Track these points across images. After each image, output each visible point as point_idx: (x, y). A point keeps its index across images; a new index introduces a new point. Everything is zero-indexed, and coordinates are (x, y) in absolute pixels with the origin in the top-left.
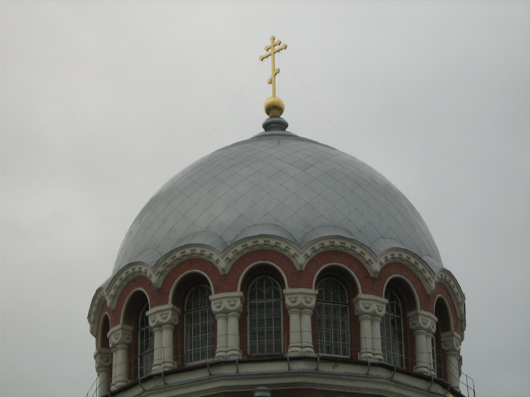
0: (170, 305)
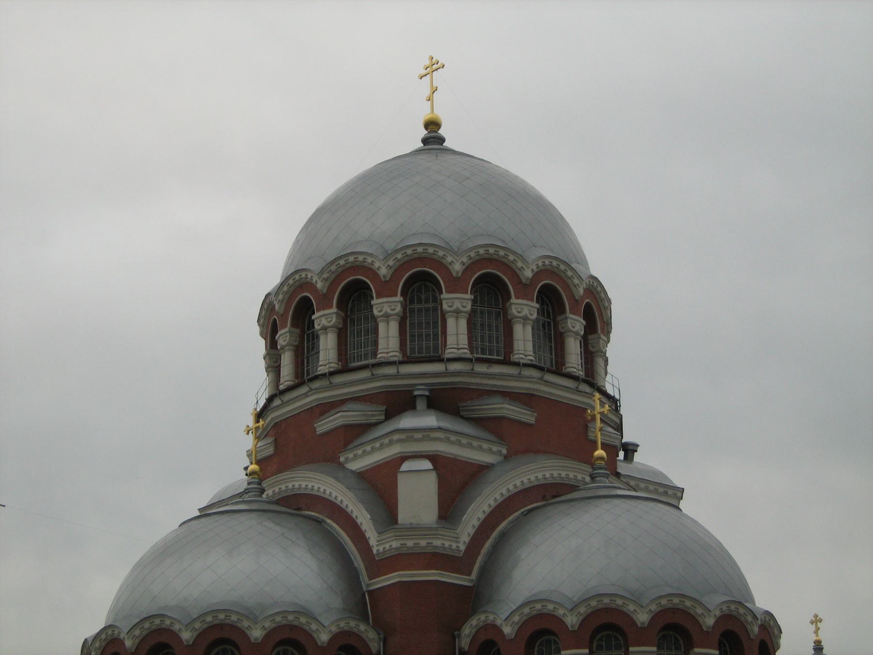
0: (334, 310)
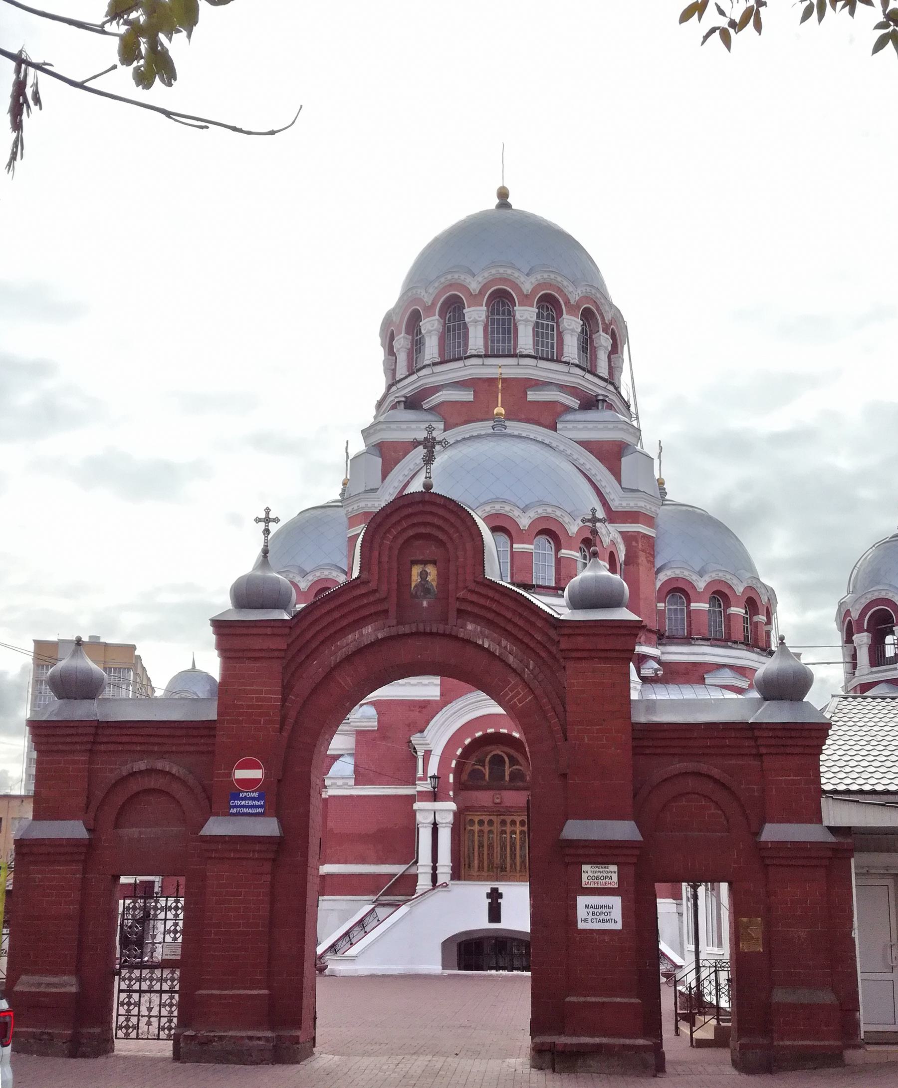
0: (437, 317)
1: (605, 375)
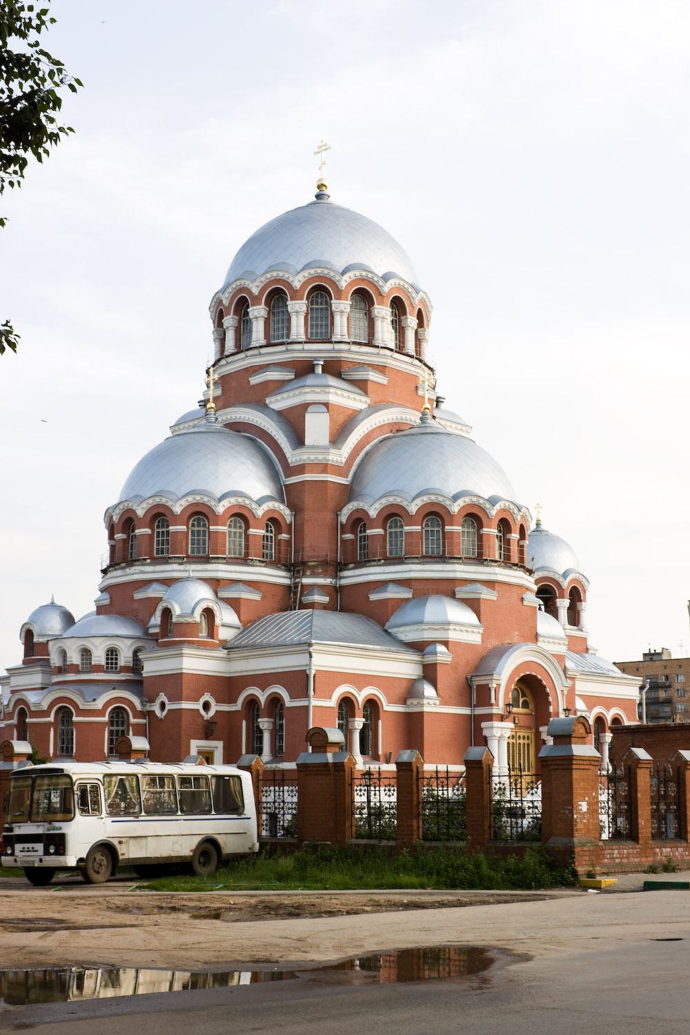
0: (263, 306)
1: (412, 352)
